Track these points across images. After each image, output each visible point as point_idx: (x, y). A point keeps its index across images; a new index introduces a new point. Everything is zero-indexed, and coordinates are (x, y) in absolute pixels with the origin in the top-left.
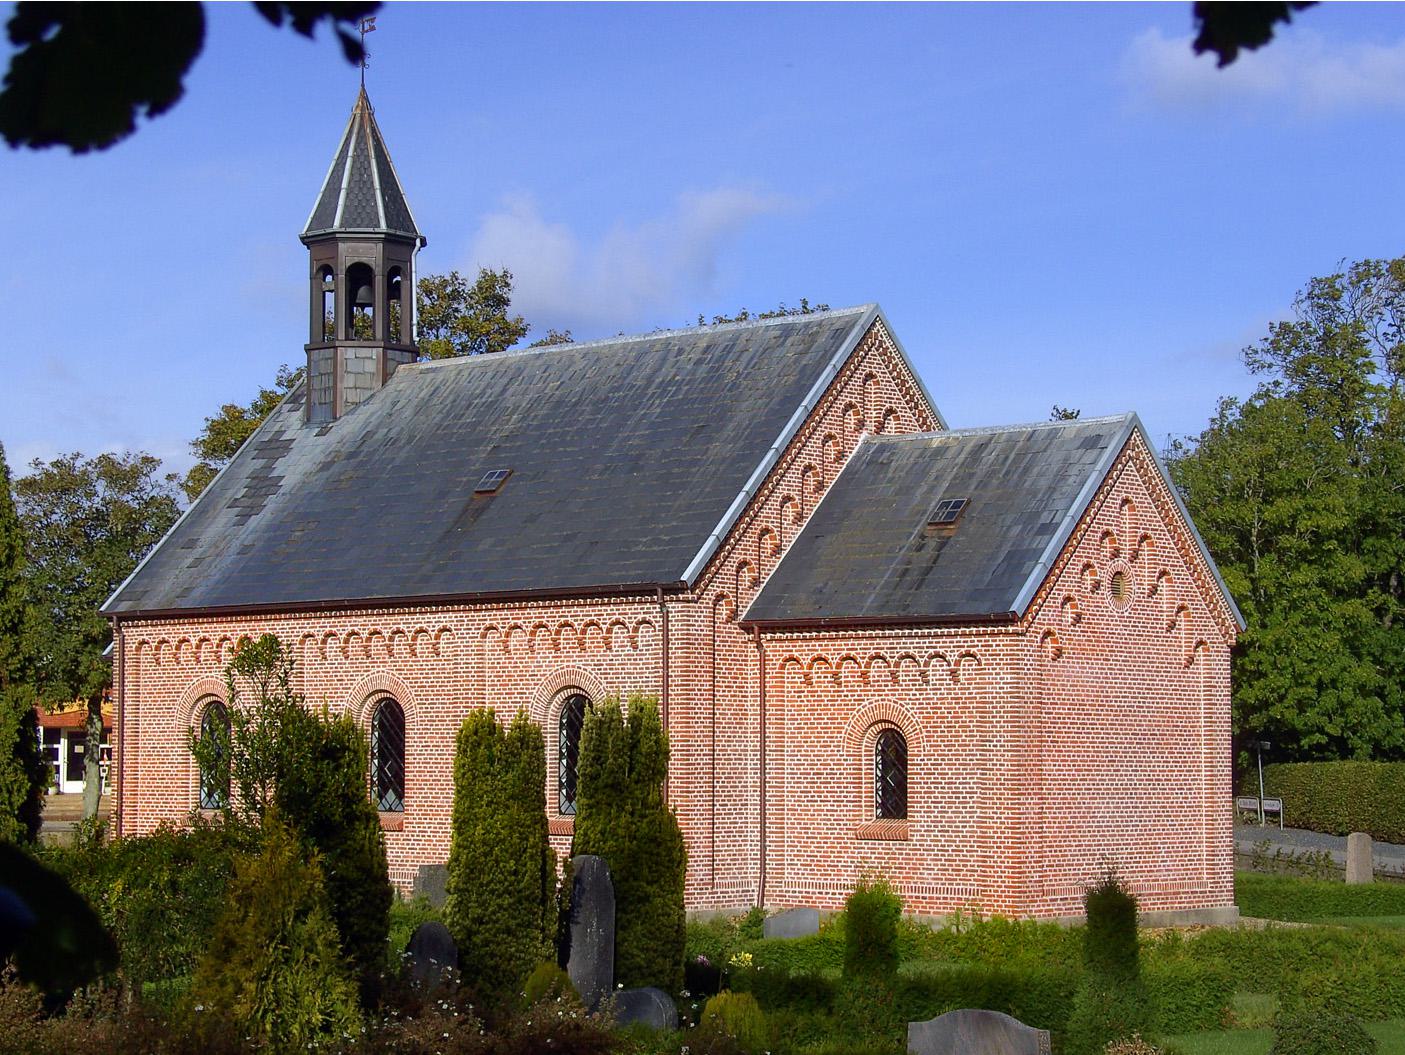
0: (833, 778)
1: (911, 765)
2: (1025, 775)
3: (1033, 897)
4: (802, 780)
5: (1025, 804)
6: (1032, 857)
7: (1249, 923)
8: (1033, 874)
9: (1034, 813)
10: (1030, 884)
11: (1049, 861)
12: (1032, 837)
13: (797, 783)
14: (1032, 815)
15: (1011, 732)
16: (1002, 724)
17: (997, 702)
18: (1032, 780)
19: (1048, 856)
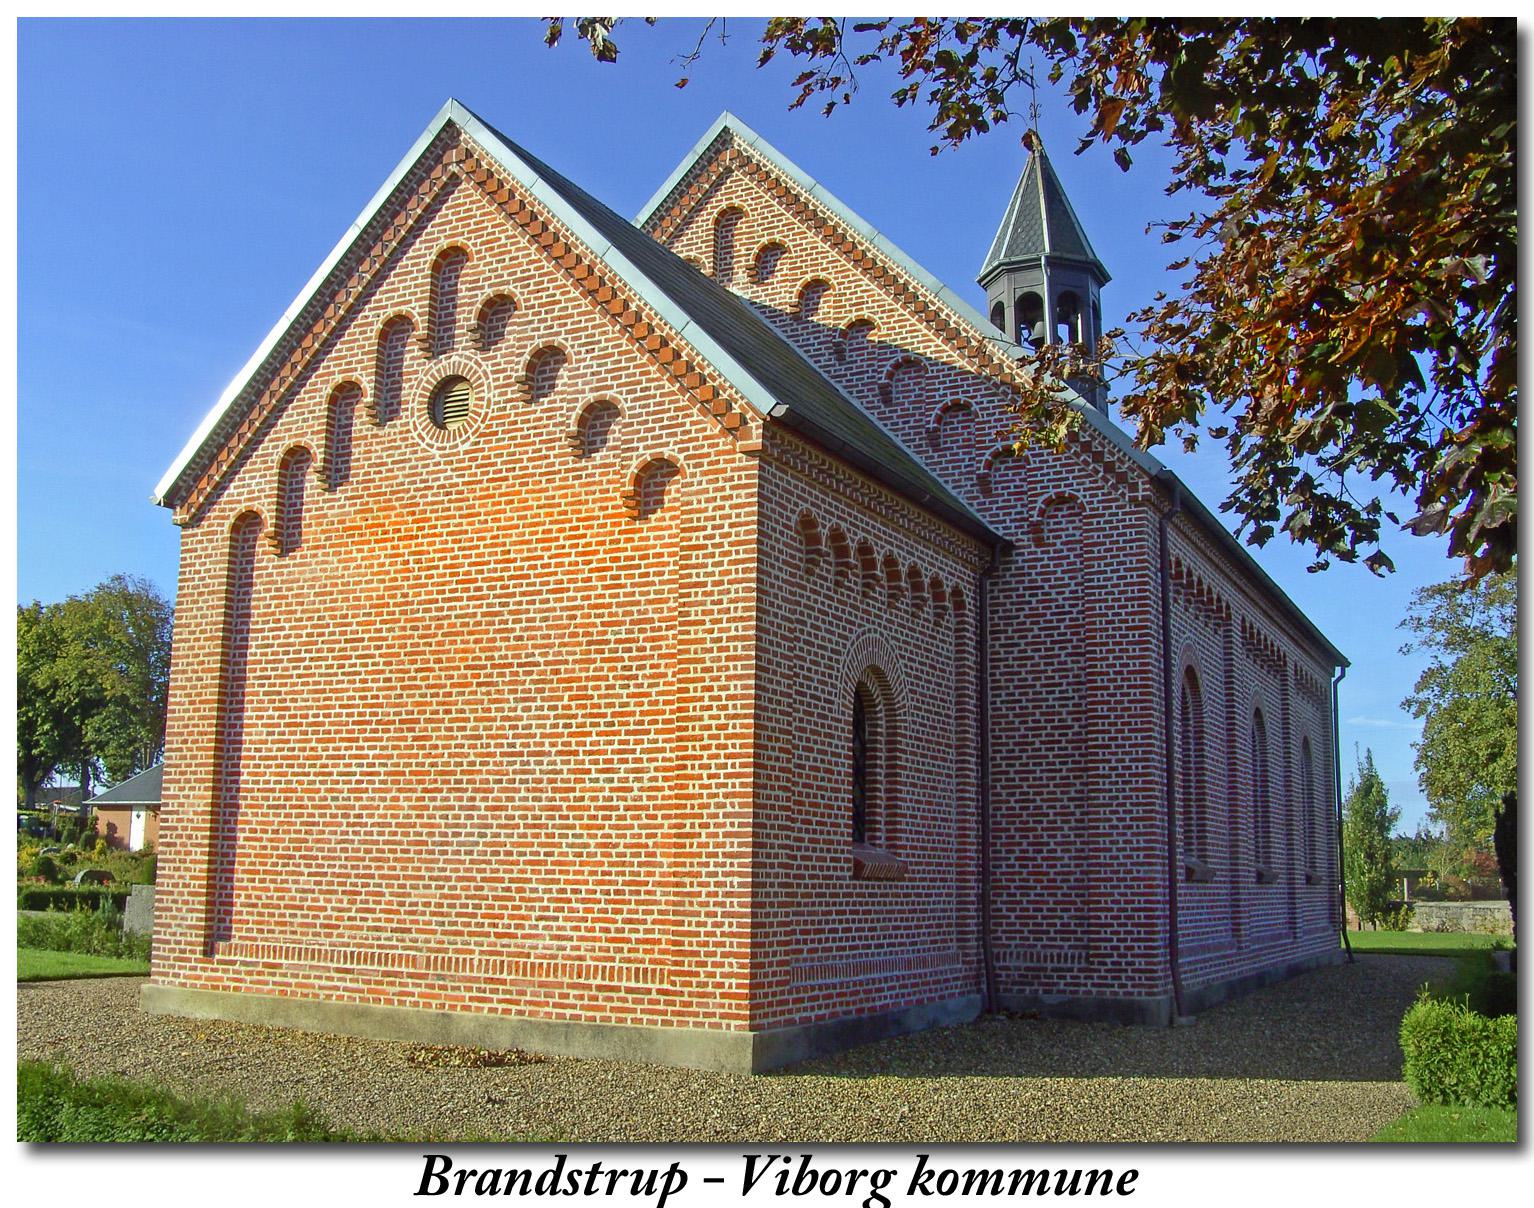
0: (512, 799)
1: (744, 835)
2: (181, 750)
3: (183, 951)
4: (273, 778)
5: (177, 797)
6: (186, 885)
7: (1409, 1069)
8: (184, 914)
9: (195, 813)
10: (179, 930)
11: (249, 897)
12: (188, 853)
13: (596, 606)
14: (191, 816)
15: (1101, 910)
16: (705, 773)
17: (711, 737)
18: (194, 757)
19: (246, 888)
